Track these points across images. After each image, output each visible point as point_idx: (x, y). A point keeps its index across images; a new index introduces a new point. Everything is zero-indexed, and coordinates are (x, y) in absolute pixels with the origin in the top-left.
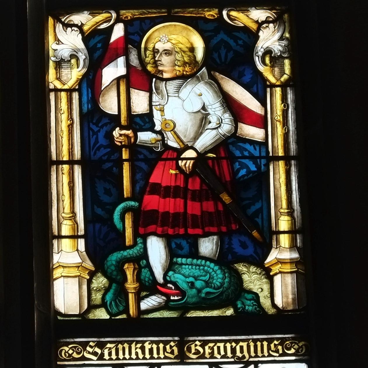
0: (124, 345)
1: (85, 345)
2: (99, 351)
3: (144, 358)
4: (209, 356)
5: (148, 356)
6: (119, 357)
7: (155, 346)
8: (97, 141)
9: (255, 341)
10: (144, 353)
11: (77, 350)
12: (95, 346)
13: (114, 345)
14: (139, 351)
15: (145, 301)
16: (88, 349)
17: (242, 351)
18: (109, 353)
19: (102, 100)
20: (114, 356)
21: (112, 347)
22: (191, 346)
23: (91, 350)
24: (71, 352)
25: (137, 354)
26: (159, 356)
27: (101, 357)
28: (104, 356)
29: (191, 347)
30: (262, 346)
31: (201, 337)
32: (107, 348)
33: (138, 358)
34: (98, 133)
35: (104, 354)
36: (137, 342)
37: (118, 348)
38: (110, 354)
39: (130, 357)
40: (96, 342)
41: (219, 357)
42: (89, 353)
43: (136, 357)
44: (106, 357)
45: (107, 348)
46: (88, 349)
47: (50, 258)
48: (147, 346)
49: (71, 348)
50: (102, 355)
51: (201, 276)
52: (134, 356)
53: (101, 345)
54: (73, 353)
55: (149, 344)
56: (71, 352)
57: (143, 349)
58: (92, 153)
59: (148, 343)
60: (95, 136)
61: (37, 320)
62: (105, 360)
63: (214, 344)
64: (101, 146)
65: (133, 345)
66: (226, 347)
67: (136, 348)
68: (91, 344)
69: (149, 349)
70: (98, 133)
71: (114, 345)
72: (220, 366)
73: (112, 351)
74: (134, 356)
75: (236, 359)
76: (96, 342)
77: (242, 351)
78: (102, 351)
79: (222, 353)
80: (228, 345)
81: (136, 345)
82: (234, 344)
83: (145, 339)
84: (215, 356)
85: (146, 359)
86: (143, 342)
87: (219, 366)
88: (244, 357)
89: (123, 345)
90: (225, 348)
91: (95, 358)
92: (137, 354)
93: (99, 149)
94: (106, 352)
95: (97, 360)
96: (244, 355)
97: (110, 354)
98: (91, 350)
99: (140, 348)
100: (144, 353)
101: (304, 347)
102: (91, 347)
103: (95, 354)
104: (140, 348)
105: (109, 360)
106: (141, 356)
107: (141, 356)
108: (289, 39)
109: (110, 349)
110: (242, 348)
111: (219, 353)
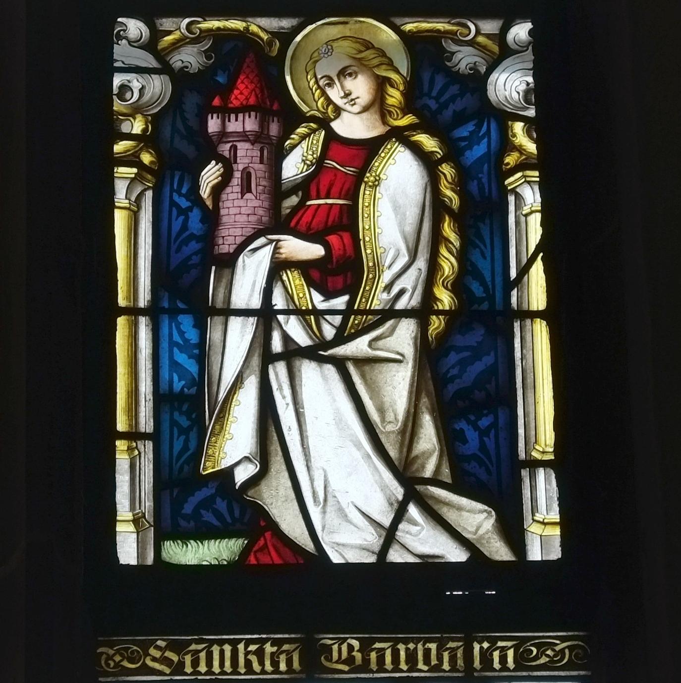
1: (145, 646)
2: (175, 658)
4: (480, 667)
5: (268, 667)
8: (184, 227)
9: (234, 643)
10: (261, 663)
11: (129, 655)
12: (166, 647)
13: (389, 644)
14: (254, 659)
15: (195, 544)
16: (153, 652)
19: (526, 351)
20: (203, 668)
21: (386, 647)
22: (333, 647)
23: (157, 654)
24: (118, 658)
25: (248, 663)
27: (179, 668)
29: (332, 648)
30: (222, 653)
34: (189, 213)
36: (248, 642)
38: (195, 663)
41: (426, 668)
42: (154, 659)
44: (188, 669)
45: (447, 649)
46: (153, 652)
48: (269, 649)
49: (118, 651)
50: (182, 664)
53: (179, 647)
54: (121, 661)
55: (272, 645)
56: (118, 658)
57: (260, 653)
58: (174, 247)
60: (182, 218)
64: (192, 237)
67: (247, 653)
68: (159, 643)
70: (189, 213)
73: (292, 655)
79: (434, 661)
80: (401, 647)
81: (246, 647)
82: (486, 645)
92: (248, 663)
93: (186, 242)
97: (195, 663)
98: (157, 654)
99: (255, 653)
100: (261, 663)
101: (567, 651)
102: (158, 648)
104: (255, 653)
106: (256, 667)
108: (302, 19)
109: (503, 650)
110: (427, 652)
111: (427, 661)
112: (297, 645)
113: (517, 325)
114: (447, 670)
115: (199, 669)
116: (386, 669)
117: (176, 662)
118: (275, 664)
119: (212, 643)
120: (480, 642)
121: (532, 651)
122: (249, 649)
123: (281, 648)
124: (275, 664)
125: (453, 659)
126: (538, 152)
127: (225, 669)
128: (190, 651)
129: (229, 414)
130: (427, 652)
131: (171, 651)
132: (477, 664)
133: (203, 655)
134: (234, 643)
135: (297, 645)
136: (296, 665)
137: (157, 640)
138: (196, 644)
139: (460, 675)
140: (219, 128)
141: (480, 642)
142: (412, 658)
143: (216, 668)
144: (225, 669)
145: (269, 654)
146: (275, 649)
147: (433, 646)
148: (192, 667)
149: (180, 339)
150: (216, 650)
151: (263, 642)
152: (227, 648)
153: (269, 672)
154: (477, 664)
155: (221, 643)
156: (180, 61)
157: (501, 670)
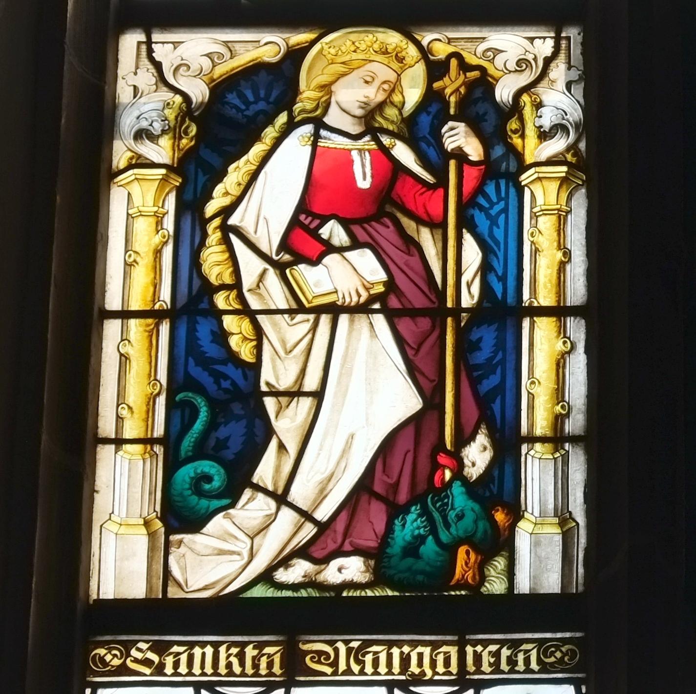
0: (205, 650)
1: (128, 646)
3: (243, 674)
6: (393, 671)
7: (505, 652)
9: (216, 645)
10: (242, 664)
12: (148, 649)
14: (235, 661)
17: (420, 664)
18: (174, 662)
20: (183, 669)
23: (139, 655)
25: (229, 665)
26: (449, 669)
28: (164, 668)
31: (560, 634)
32: (521, 650)
33: (231, 673)
35: (165, 664)
37: (193, 654)
38: (176, 665)
39: (270, 671)
40: (151, 643)
42: (136, 661)
43: (387, 670)
44: (169, 670)
46: (134, 653)
47: (101, 204)
48: (250, 652)
51: (423, 374)
52: (222, 670)
55: (254, 648)
57: (241, 656)
59: (251, 646)
61: (35, 584)
62: (165, 675)
63: (498, 646)
65: (222, 649)
66: (392, 654)
69: (508, 657)
71: (185, 648)
72: (412, 688)
74: (222, 670)
75: (409, 675)
76: (151, 643)
77: (420, 664)
78: (160, 660)
80: (396, 651)
81: (228, 649)
83: (245, 639)
84: (482, 669)
85: (246, 676)
86: (243, 645)
87: (216, 690)
88: (423, 673)
89: (400, 648)
90: (390, 657)
91: (148, 671)
92: (229, 665)
94: (169, 661)
95: (152, 675)
96: (423, 670)
97: (176, 665)
100: (242, 664)
103: (147, 662)
105: (201, 675)
106: (237, 669)
107: (237, 669)
109: (527, 652)
110: (420, 656)
112: (535, 645)
113: (526, 323)
114: (278, 674)
115: (274, 670)
116: (219, 673)
117: (156, 663)
118: (256, 666)
119: (191, 645)
120: (474, 646)
121: (324, 659)
122: (230, 652)
123: (262, 651)
124: (256, 666)
125: (447, 662)
126: (390, 153)
127: (205, 671)
128: (521, 650)
129: (451, 426)
130: (420, 656)
131: (152, 651)
132: (471, 668)
133: (184, 658)
134: (216, 645)
135: (535, 645)
136: (277, 669)
137: (338, 641)
138: (179, 645)
139: (453, 677)
140: (480, 155)
141: (474, 646)
142: (405, 661)
143: (197, 670)
144: (205, 671)
145: (251, 658)
146: (256, 652)
147: (427, 651)
148: (245, 652)
149: (217, 368)
150: (197, 651)
151: (243, 645)
152: (209, 650)
153: (487, 672)
154: (471, 668)
155: (203, 644)
156: (144, 119)
157: (386, 674)
